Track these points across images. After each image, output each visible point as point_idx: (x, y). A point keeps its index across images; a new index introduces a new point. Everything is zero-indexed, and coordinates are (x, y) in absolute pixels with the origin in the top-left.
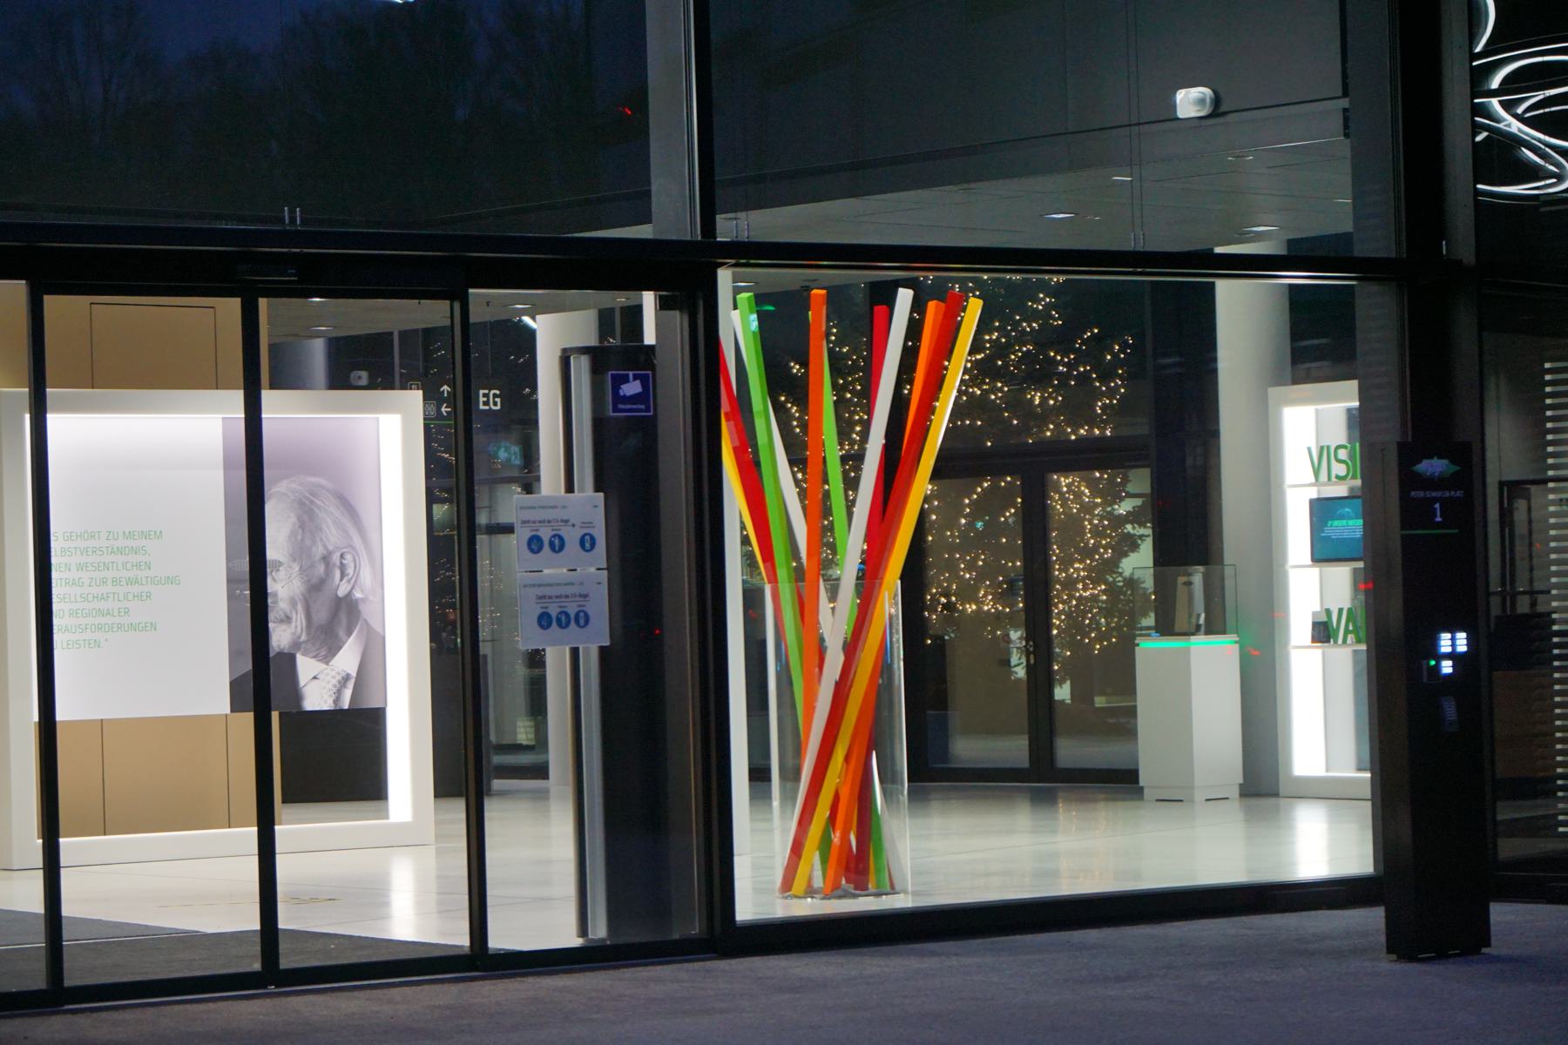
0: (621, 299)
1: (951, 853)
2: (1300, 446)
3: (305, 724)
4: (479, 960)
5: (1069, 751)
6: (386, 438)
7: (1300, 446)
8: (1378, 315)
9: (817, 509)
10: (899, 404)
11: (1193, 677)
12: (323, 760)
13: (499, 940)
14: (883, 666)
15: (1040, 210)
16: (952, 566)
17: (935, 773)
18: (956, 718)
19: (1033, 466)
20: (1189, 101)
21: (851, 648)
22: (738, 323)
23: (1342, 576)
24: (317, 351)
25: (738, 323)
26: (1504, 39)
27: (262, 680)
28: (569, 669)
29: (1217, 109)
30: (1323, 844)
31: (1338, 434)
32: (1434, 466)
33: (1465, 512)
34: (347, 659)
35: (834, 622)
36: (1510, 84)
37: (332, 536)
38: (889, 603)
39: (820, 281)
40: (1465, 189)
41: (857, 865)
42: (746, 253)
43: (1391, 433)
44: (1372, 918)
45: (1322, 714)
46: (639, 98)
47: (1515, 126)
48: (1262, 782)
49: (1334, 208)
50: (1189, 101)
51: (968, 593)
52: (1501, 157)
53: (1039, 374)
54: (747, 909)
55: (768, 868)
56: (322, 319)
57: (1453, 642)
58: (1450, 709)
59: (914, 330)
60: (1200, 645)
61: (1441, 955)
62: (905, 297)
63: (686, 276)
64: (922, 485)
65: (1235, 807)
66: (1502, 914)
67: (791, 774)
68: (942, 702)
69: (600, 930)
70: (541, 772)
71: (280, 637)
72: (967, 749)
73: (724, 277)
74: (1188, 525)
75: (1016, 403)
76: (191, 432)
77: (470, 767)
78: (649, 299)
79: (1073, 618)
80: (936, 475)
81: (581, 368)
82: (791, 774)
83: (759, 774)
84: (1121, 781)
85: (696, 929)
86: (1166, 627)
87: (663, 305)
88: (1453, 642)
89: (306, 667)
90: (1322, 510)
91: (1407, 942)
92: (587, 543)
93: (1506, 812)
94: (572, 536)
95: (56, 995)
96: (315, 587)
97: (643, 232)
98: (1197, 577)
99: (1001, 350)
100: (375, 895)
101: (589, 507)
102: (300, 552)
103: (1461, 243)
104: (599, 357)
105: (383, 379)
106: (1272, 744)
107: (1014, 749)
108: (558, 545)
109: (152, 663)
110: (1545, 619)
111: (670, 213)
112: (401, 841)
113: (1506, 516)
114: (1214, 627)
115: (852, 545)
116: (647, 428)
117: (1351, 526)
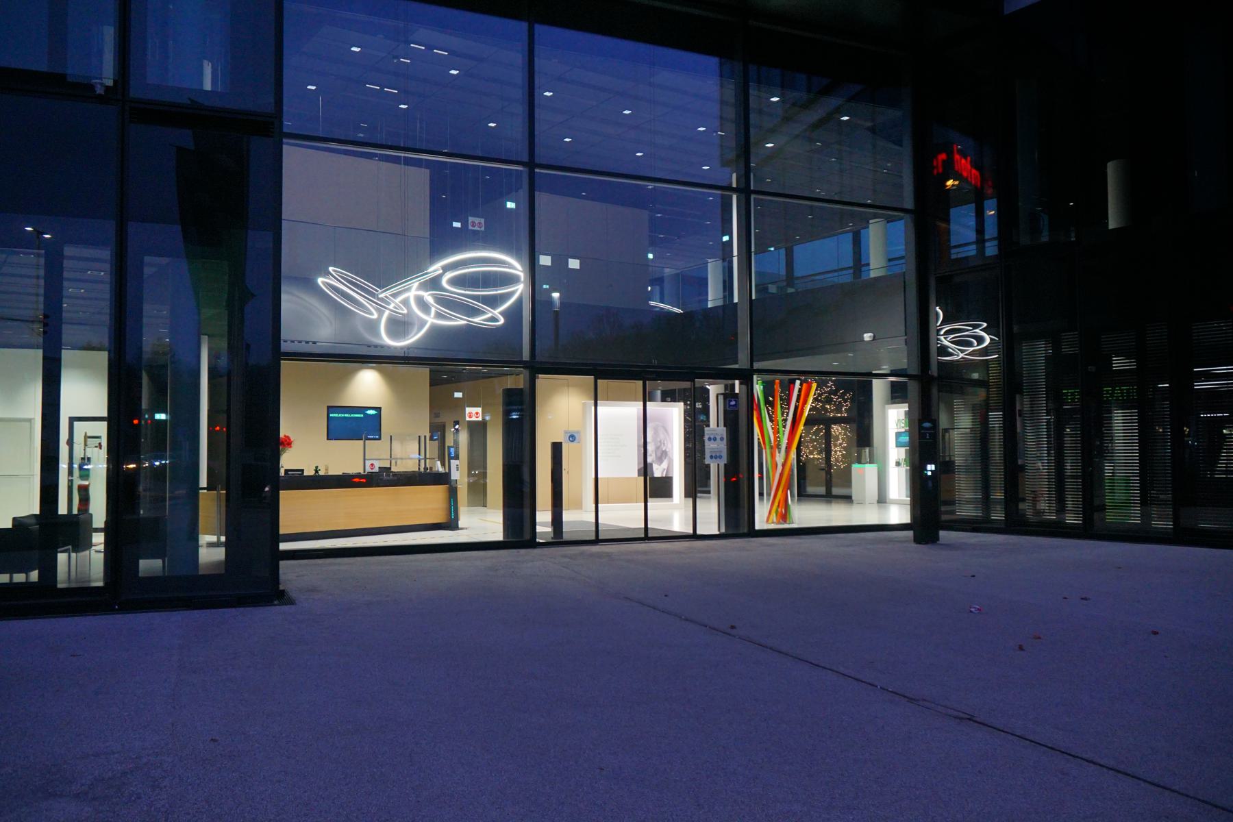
0: (730, 382)
1: (807, 515)
2: (892, 420)
3: (654, 479)
4: (695, 536)
5: (835, 491)
6: (673, 415)
7: (892, 420)
8: (913, 387)
9: (776, 431)
10: (796, 408)
11: (865, 475)
12: (657, 488)
13: (699, 532)
14: (791, 470)
15: (833, 362)
16: (807, 447)
17: (803, 495)
18: (808, 482)
19: (828, 423)
20: (867, 337)
21: (784, 465)
22: (758, 388)
23: (903, 450)
24: (659, 393)
25: (758, 388)
26: (944, 322)
27: (645, 470)
28: (716, 469)
29: (874, 338)
30: (898, 514)
31: (902, 416)
32: (927, 425)
33: (934, 436)
34: (665, 465)
35: (780, 459)
36: (948, 333)
37: (662, 436)
38: (793, 455)
39: (777, 379)
40: (935, 358)
41: (784, 517)
42: (760, 372)
43: (916, 416)
44: (910, 533)
45: (898, 483)
46: (736, 335)
47: (947, 343)
48: (882, 500)
49: (903, 363)
50: (867, 337)
51: (811, 453)
52: (943, 351)
53: (829, 401)
54: (757, 527)
55: (763, 517)
56: (659, 387)
57: (931, 467)
58: (930, 484)
59: (800, 390)
60: (867, 466)
61: (927, 543)
62: (798, 382)
63: (746, 377)
64: (801, 427)
65: (876, 505)
66: (942, 533)
67: (769, 495)
68: (804, 479)
69: (723, 530)
70: (709, 492)
71: (649, 460)
72: (810, 490)
73: (755, 377)
74: (864, 438)
75: (823, 408)
76: (632, 410)
77: (696, 485)
78: (737, 382)
79: (837, 460)
80: (805, 424)
81: (721, 398)
82: (769, 495)
83: (761, 494)
84: (848, 499)
85: (746, 531)
86: (860, 463)
87: (741, 384)
88: (931, 467)
89: (655, 466)
90: (898, 435)
91: (917, 540)
92: (722, 439)
93: (943, 509)
94: (718, 438)
95: (597, 541)
96: (658, 448)
97: (736, 366)
98: (867, 450)
99: (820, 395)
100: (669, 520)
101: (722, 430)
102: (654, 440)
103: (934, 371)
104: (725, 396)
105: (674, 400)
106: (884, 490)
107: (822, 490)
108: (715, 439)
109: (620, 465)
110: (953, 462)
111: (743, 362)
112: (676, 507)
113: (943, 436)
114: (871, 462)
115: (784, 441)
116: (736, 413)
117: (906, 439)
